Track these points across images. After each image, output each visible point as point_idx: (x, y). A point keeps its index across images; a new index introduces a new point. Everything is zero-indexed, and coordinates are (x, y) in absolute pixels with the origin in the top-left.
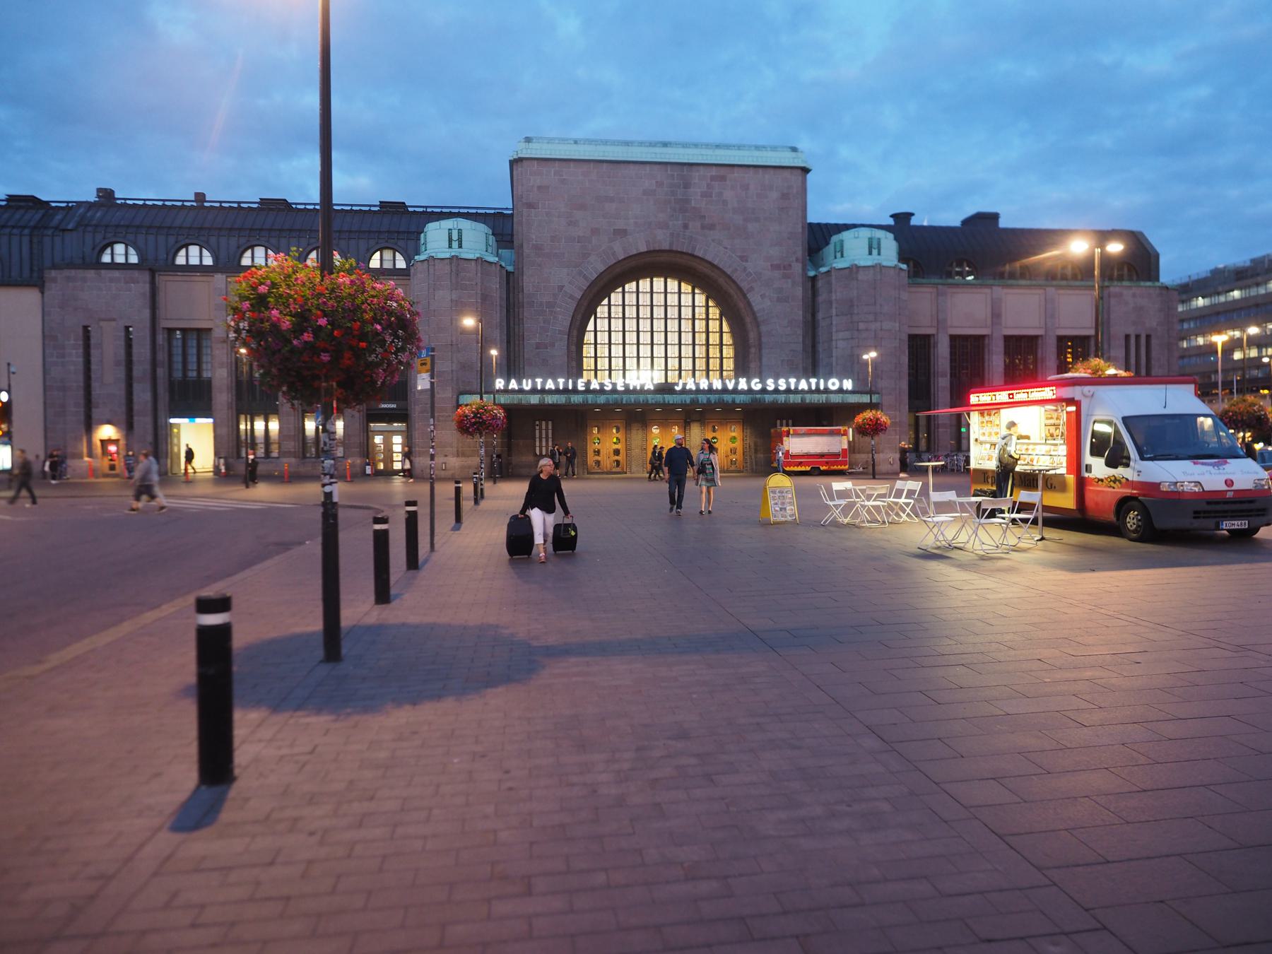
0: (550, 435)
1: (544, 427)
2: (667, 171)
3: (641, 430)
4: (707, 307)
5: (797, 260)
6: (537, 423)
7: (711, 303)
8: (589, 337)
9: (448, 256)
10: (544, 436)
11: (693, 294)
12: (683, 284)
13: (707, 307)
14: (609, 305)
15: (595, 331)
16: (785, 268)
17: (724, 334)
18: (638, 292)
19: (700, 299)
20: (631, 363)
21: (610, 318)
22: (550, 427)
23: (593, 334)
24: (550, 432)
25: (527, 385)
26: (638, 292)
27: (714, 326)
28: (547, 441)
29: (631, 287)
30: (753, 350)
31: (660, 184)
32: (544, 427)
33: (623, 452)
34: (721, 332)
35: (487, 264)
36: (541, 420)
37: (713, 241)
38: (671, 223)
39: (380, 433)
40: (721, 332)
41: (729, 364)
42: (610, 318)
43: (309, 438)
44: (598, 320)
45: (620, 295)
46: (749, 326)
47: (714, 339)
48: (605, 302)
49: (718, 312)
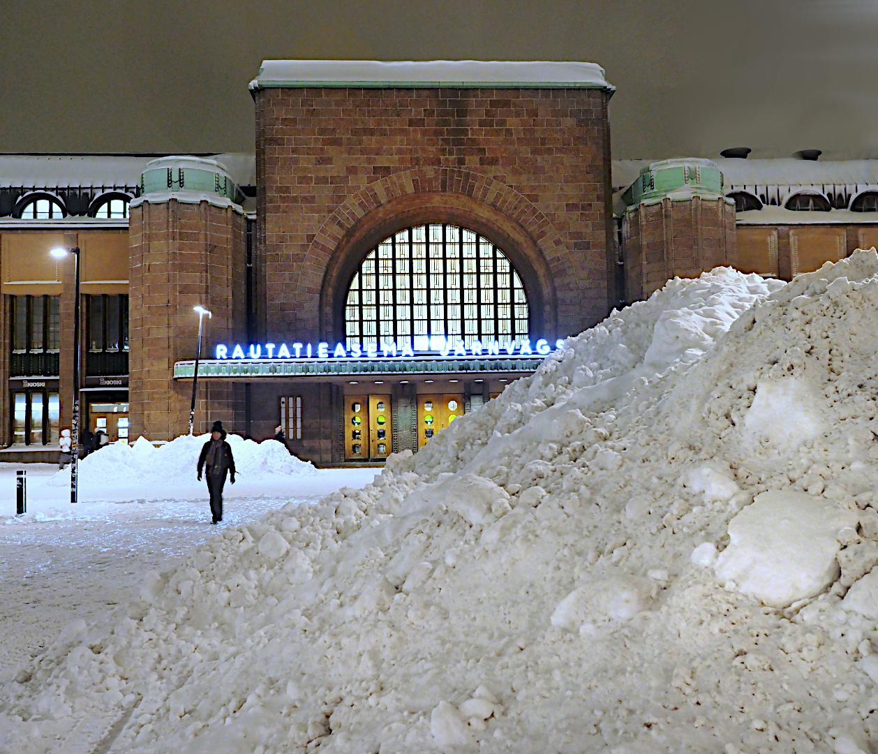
0: (299, 415)
1: (291, 404)
2: (438, 97)
3: (409, 408)
4: (495, 259)
5: (599, 198)
6: (283, 399)
7: (499, 255)
8: (353, 297)
9: (165, 198)
10: (291, 415)
11: (478, 243)
12: (465, 232)
13: (495, 259)
14: (377, 260)
15: (360, 290)
16: (583, 208)
17: (516, 292)
18: (411, 243)
19: (486, 250)
20: (420, 327)
21: (377, 274)
22: (299, 405)
23: (357, 293)
24: (299, 410)
25: (255, 352)
26: (411, 243)
27: (503, 281)
28: (295, 422)
29: (402, 237)
30: (547, 308)
31: (429, 113)
32: (291, 404)
33: (388, 434)
34: (512, 289)
35: (214, 210)
36: (287, 397)
37: (494, 178)
38: (442, 157)
39: (103, 415)
40: (512, 289)
41: (522, 326)
42: (377, 274)
43: (19, 423)
44: (364, 278)
45: (390, 247)
46: (542, 280)
47: (504, 296)
48: (372, 255)
49: (508, 264)
